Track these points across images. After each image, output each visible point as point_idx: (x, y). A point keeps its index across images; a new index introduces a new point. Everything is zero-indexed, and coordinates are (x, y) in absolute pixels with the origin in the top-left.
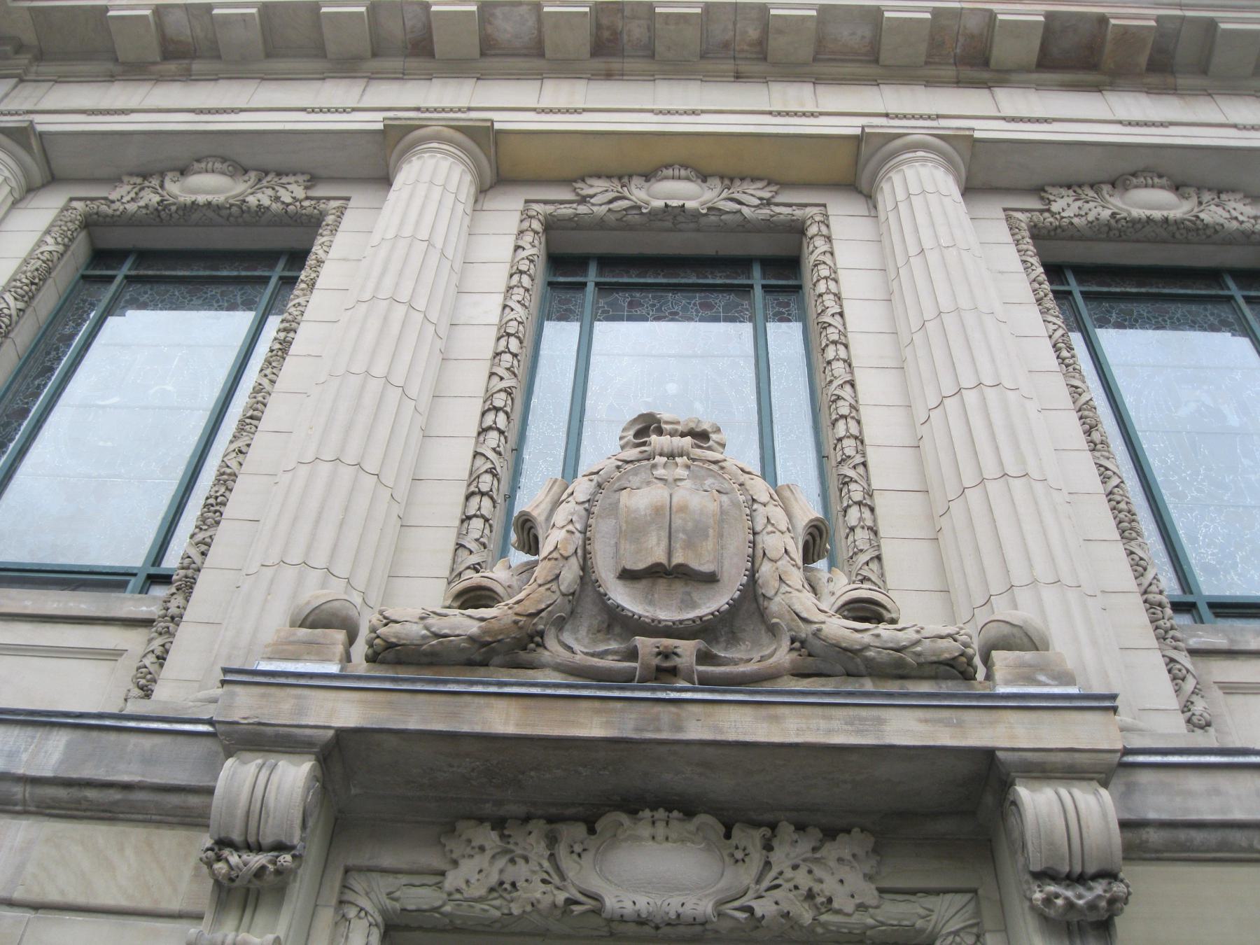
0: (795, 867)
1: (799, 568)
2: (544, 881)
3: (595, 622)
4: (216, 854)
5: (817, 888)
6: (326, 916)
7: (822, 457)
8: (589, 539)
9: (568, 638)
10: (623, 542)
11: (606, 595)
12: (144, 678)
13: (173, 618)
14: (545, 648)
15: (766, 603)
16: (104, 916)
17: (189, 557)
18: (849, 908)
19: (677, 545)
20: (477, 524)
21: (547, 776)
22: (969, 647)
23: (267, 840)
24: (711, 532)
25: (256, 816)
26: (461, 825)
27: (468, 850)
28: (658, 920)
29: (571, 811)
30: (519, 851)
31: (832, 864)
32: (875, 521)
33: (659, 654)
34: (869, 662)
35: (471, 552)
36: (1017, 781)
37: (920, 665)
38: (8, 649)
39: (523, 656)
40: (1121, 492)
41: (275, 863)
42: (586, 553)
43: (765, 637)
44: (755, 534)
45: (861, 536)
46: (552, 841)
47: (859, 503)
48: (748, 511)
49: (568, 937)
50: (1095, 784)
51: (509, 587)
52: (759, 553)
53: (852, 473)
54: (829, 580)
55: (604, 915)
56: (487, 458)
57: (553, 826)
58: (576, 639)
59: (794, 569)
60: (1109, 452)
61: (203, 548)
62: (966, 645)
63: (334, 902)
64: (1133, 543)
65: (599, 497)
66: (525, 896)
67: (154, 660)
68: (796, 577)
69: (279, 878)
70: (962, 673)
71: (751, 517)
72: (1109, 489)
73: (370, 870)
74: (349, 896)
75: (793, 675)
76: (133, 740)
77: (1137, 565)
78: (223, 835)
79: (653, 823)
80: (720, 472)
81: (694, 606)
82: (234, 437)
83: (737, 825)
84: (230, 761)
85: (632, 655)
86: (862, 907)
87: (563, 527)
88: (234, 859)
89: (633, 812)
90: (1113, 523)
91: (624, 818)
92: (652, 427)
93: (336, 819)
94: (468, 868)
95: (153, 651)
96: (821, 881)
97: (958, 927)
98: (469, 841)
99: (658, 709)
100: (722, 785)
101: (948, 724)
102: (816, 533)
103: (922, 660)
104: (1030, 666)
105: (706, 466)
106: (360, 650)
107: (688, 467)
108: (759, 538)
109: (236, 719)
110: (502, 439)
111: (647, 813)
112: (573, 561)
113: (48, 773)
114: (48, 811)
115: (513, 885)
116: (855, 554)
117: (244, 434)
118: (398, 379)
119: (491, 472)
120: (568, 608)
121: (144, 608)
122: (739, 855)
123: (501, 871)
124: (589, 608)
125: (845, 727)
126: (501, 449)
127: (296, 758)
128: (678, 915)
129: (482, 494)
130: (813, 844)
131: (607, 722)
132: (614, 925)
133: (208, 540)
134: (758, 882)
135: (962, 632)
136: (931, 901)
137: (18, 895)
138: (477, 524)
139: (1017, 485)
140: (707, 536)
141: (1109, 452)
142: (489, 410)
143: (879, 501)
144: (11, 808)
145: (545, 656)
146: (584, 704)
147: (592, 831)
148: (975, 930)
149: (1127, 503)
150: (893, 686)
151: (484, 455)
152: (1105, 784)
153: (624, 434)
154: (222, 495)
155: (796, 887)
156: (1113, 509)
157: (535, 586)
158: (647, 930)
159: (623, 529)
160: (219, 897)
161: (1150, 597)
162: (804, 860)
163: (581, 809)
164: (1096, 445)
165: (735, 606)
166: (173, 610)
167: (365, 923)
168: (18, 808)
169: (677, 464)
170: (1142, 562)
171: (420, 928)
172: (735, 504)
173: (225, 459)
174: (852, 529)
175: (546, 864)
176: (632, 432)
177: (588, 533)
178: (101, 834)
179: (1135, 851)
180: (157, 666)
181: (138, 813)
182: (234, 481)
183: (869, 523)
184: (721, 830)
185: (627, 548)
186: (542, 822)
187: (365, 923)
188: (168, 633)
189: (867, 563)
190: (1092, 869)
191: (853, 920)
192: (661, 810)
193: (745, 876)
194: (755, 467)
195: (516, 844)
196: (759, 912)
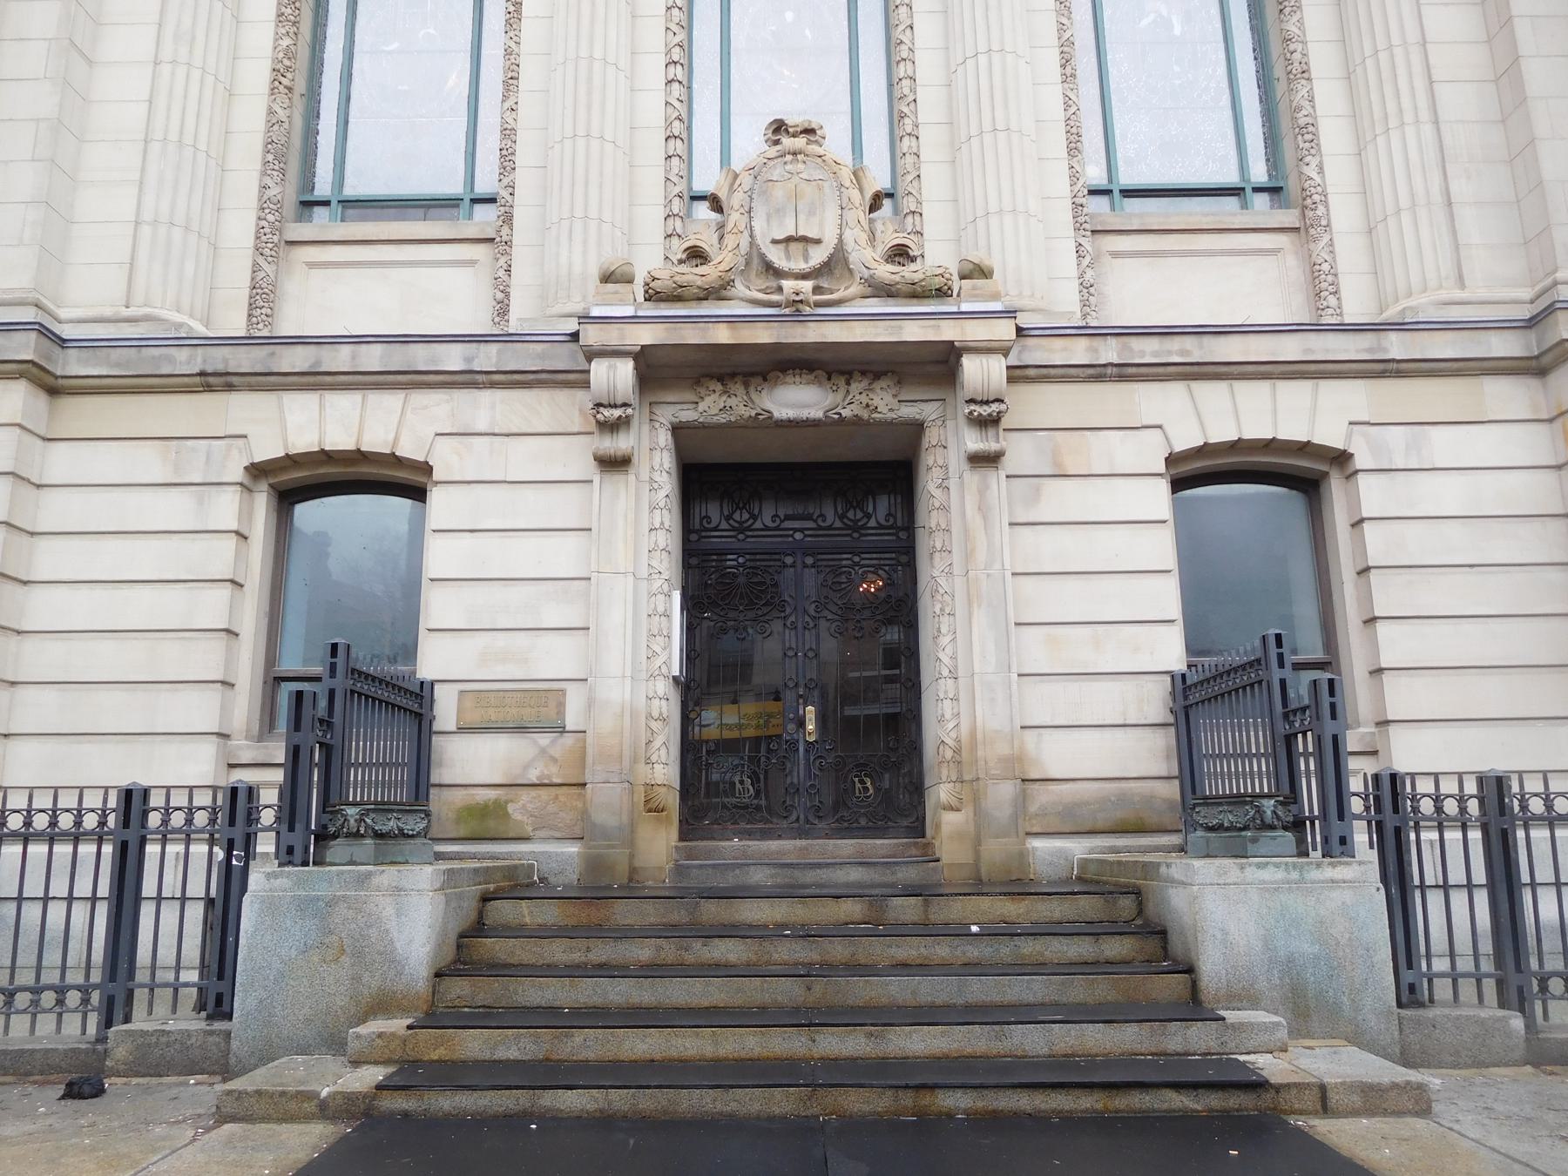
0: (860, 393)
2: (745, 405)
7: (890, 85)
20: (675, 161)
27: (708, 392)
31: (879, 391)
36: (964, 355)
45: (910, 159)
47: (909, 134)
50: (1000, 355)
53: (906, 110)
63: (648, 421)
74: (655, 417)
85: (780, 289)
90: (1065, 144)
94: (709, 401)
98: (708, 387)
102: (877, 198)
115: (731, 407)
117: (511, 94)
118: (611, 59)
133: (511, 184)
134: (844, 400)
138: (675, 161)
142: (670, 63)
143: (922, 132)
148: (943, 419)
155: (861, 403)
158: (793, 424)
161: (1076, 200)
166: (505, 238)
170: (1077, 175)
175: (745, 397)
176: (771, 131)
190: (991, 399)
196: (844, 415)
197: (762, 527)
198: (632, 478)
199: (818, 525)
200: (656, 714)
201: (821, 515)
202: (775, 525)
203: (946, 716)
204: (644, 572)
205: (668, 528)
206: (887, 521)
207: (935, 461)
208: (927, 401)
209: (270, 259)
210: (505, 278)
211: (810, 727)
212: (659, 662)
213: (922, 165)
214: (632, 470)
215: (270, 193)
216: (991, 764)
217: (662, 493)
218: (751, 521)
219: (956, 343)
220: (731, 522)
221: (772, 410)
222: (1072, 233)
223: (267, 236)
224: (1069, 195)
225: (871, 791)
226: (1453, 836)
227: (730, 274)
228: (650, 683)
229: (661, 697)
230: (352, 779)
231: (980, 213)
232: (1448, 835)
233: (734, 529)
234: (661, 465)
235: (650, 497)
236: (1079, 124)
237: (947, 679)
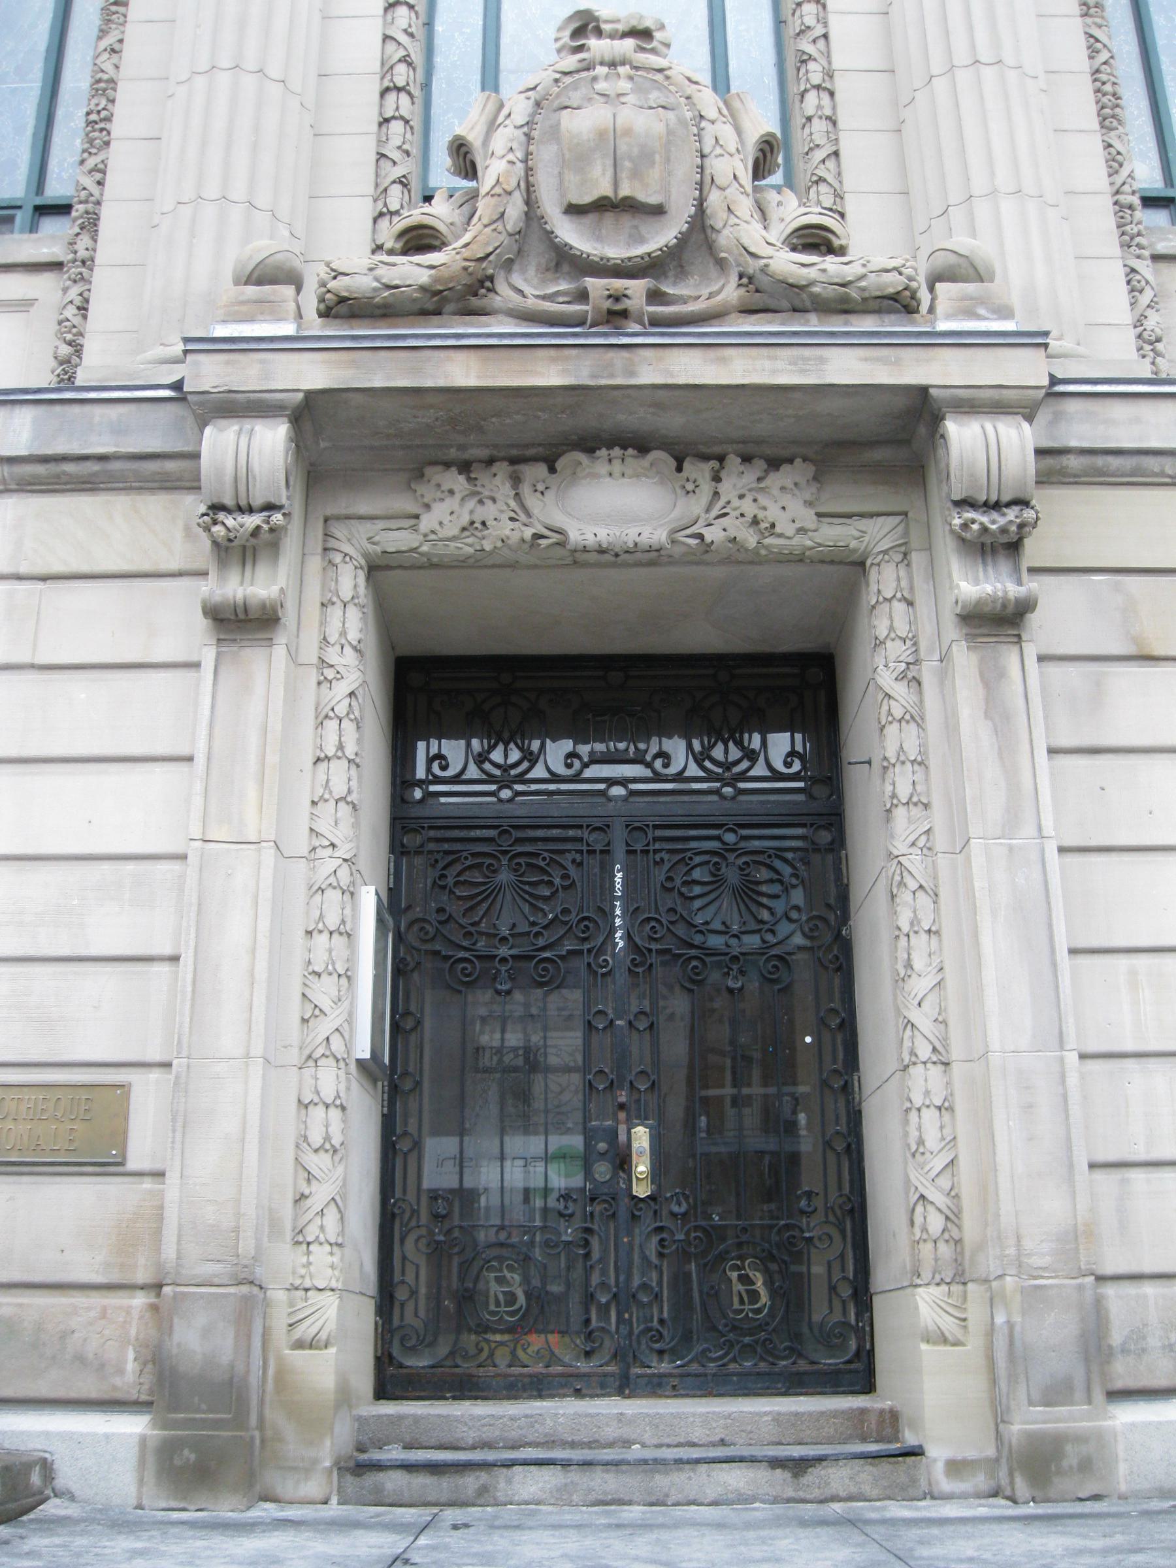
0: (741, 497)
1: (748, 195)
2: (511, 519)
3: (543, 261)
5: (761, 515)
6: (315, 563)
8: (532, 170)
9: (517, 280)
10: (566, 171)
11: (553, 232)
12: (70, 332)
13: (83, 262)
14: (496, 293)
15: (714, 236)
17: (84, 189)
18: (790, 533)
19: (624, 175)
21: (508, 421)
22: (914, 280)
23: (257, 502)
24: (657, 157)
25: (244, 480)
26: (429, 471)
27: (439, 495)
28: (617, 550)
29: (531, 452)
30: (486, 493)
31: (775, 492)
32: (834, 108)
33: (610, 296)
34: (815, 298)
35: (395, 163)
36: (948, 415)
37: (864, 300)
39: (475, 302)
40: (1109, 71)
41: (268, 523)
42: (529, 186)
43: (713, 271)
44: (703, 156)
45: (819, 126)
46: (516, 480)
47: (818, 87)
48: (695, 130)
49: (536, 566)
50: (1019, 418)
51: (452, 224)
52: (708, 180)
53: (810, 49)
54: (779, 204)
55: (568, 547)
56: (399, 44)
57: (516, 467)
58: (525, 280)
59: (743, 197)
60: (1103, 17)
61: (98, 176)
62: (910, 279)
63: (320, 550)
64: (1113, 133)
65: (538, 118)
66: (495, 533)
67: (76, 311)
68: (745, 206)
69: (273, 535)
70: (905, 307)
71: (699, 136)
72: (1096, 67)
73: (348, 517)
74: (332, 543)
75: (741, 312)
76: (98, 411)
77: (1113, 160)
78: (215, 500)
79: (610, 460)
80: (666, 83)
81: (642, 240)
82: (101, 31)
83: (688, 459)
84: (208, 431)
85: (582, 296)
86: (802, 531)
87: (503, 157)
88: (230, 522)
89: (590, 451)
90: (1093, 109)
91: (581, 457)
92: (590, 27)
93: (309, 472)
95: (71, 302)
96: (765, 509)
97: (887, 547)
98: (439, 486)
99: (611, 354)
100: (673, 423)
101: (885, 361)
102: (767, 148)
103: (866, 295)
104: (972, 299)
105: (650, 76)
106: (311, 306)
107: (631, 78)
108: (707, 162)
110: (413, 15)
111: (603, 452)
112: (517, 194)
113: (24, 452)
114: (29, 488)
115: (484, 523)
116: (811, 149)
117: (113, 26)
119: (406, 61)
120: (515, 248)
121: (45, 250)
122: (690, 487)
123: (471, 512)
124: (536, 246)
125: (790, 367)
126: (413, 30)
128: (636, 544)
129: (399, 89)
130: (759, 474)
131: (563, 370)
132: (577, 555)
133: (101, 166)
134: (708, 511)
135: (908, 264)
136: (864, 524)
137: (23, 569)
138: (397, 127)
139: (988, 73)
140: (653, 163)
141: (1103, 17)
143: (840, 85)
145: (496, 301)
146: (541, 353)
147: (552, 470)
148: (903, 549)
149: (1114, 84)
150: (836, 324)
151: (395, 40)
152: (1030, 418)
153: (559, 35)
154: (104, 109)
155: (742, 515)
156: (1098, 91)
157: (479, 226)
158: (608, 557)
159: (567, 156)
161: (1121, 198)
162: (750, 490)
163: (541, 449)
164: (1089, 8)
165: (683, 240)
166: (82, 253)
167: (350, 567)
169: (618, 75)
170: (1119, 158)
171: (400, 567)
172: (682, 122)
173: (97, 62)
174: (809, 119)
175: (513, 504)
176: (567, 33)
177: (530, 163)
179: (1045, 479)
180: (79, 318)
182: (115, 90)
183: (828, 112)
184: (673, 464)
185: (571, 178)
186: (506, 464)
187: (350, 567)
188: (80, 279)
189: (823, 161)
190: (1006, 498)
191: (794, 542)
192: (617, 449)
193: (696, 506)
194: (705, 78)
195: (483, 486)
196: (708, 539)
197: (546, 775)
198: (279, 652)
199: (654, 771)
200: (316, 1138)
201: (662, 754)
202: (570, 772)
203: (927, 1144)
204: (300, 843)
205: (352, 757)
206: (788, 765)
207: (891, 628)
208: (872, 515)
210: (77, 321)
211: (642, 1168)
212: (324, 1027)
213: (842, 135)
214: (281, 640)
216: (1028, 1244)
217: (342, 689)
218: (525, 765)
219: (931, 391)
220: (487, 766)
221: (566, 527)
222: (1117, 251)
224: (1109, 190)
225: (764, 1298)
227: (484, 265)
228: (308, 1072)
229: (329, 1101)
231: (954, 197)
233: (491, 779)
234: (343, 633)
235: (318, 696)
236: (1113, 79)
237: (929, 1065)
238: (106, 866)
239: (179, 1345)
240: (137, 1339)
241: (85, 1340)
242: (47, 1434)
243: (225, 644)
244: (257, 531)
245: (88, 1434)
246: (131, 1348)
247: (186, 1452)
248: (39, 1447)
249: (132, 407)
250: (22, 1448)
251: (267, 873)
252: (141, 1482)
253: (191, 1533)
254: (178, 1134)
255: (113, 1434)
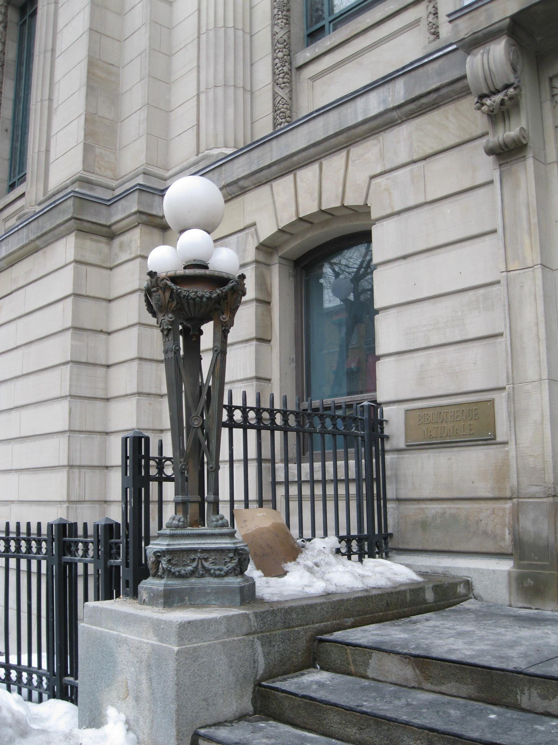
4: (481, 103)
12: (432, 28)
16: (452, 150)
38: (334, 67)
63: (549, 97)
78: (480, 93)
95: (430, 13)
109: (462, 37)
113: (402, 101)
114: (411, 117)
127: (498, 40)
137: (415, 157)
144: (396, 123)
160: (492, 121)
168: (399, 121)
178: (435, 116)
180: (435, 19)
181: (448, 99)
198: (530, 162)
209: (283, 85)
214: (530, 155)
215: (278, 37)
223: (279, 69)
226: (238, 433)
230: (375, 492)
232: (339, 463)
238: (471, 293)
239: (523, 528)
240: (509, 524)
241: (487, 524)
242: (468, 569)
243: (503, 166)
244: (502, 102)
245: (485, 570)
246: (507, 529)
247: (529, 580)
248: (466, 575)
249: (444, 59)
250: (459, 575)
251: (539, 282)
252: (510, 593)
253: (555, 617)
254: (512, 423)
255: (496, 570)
